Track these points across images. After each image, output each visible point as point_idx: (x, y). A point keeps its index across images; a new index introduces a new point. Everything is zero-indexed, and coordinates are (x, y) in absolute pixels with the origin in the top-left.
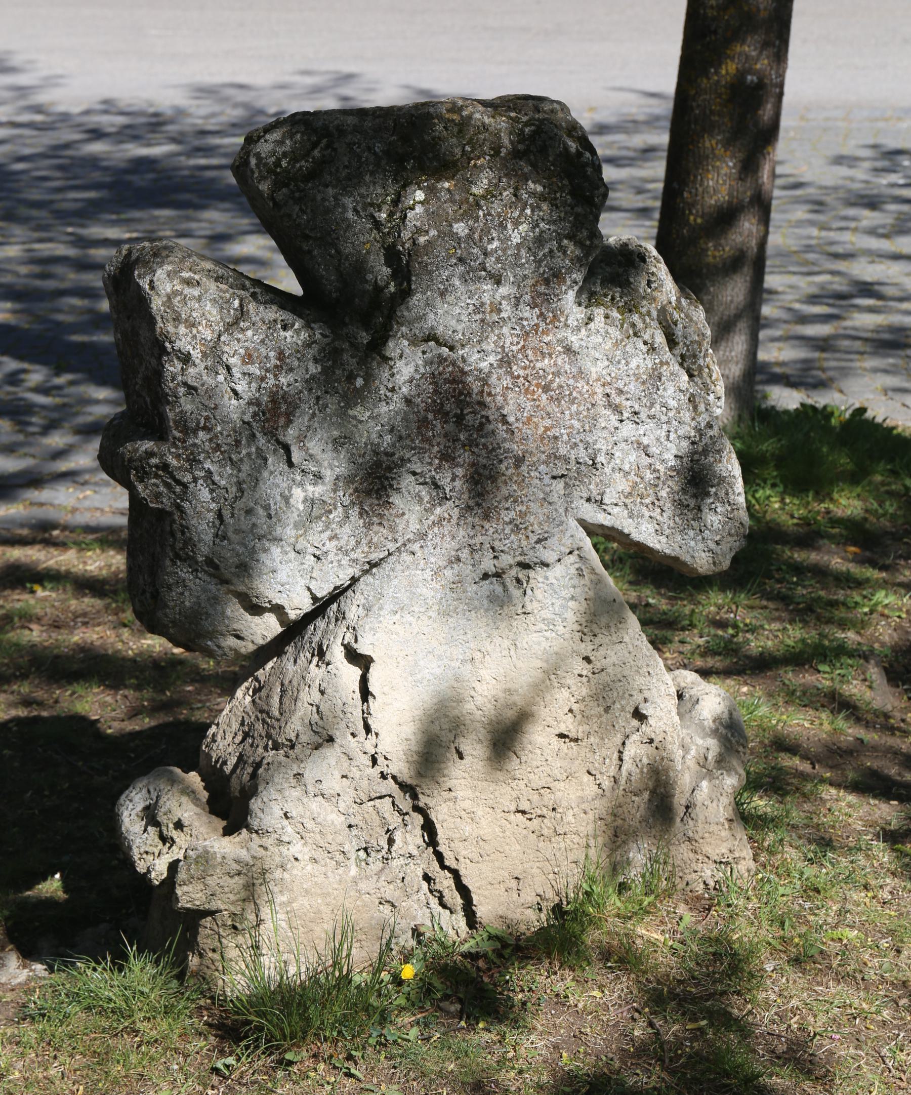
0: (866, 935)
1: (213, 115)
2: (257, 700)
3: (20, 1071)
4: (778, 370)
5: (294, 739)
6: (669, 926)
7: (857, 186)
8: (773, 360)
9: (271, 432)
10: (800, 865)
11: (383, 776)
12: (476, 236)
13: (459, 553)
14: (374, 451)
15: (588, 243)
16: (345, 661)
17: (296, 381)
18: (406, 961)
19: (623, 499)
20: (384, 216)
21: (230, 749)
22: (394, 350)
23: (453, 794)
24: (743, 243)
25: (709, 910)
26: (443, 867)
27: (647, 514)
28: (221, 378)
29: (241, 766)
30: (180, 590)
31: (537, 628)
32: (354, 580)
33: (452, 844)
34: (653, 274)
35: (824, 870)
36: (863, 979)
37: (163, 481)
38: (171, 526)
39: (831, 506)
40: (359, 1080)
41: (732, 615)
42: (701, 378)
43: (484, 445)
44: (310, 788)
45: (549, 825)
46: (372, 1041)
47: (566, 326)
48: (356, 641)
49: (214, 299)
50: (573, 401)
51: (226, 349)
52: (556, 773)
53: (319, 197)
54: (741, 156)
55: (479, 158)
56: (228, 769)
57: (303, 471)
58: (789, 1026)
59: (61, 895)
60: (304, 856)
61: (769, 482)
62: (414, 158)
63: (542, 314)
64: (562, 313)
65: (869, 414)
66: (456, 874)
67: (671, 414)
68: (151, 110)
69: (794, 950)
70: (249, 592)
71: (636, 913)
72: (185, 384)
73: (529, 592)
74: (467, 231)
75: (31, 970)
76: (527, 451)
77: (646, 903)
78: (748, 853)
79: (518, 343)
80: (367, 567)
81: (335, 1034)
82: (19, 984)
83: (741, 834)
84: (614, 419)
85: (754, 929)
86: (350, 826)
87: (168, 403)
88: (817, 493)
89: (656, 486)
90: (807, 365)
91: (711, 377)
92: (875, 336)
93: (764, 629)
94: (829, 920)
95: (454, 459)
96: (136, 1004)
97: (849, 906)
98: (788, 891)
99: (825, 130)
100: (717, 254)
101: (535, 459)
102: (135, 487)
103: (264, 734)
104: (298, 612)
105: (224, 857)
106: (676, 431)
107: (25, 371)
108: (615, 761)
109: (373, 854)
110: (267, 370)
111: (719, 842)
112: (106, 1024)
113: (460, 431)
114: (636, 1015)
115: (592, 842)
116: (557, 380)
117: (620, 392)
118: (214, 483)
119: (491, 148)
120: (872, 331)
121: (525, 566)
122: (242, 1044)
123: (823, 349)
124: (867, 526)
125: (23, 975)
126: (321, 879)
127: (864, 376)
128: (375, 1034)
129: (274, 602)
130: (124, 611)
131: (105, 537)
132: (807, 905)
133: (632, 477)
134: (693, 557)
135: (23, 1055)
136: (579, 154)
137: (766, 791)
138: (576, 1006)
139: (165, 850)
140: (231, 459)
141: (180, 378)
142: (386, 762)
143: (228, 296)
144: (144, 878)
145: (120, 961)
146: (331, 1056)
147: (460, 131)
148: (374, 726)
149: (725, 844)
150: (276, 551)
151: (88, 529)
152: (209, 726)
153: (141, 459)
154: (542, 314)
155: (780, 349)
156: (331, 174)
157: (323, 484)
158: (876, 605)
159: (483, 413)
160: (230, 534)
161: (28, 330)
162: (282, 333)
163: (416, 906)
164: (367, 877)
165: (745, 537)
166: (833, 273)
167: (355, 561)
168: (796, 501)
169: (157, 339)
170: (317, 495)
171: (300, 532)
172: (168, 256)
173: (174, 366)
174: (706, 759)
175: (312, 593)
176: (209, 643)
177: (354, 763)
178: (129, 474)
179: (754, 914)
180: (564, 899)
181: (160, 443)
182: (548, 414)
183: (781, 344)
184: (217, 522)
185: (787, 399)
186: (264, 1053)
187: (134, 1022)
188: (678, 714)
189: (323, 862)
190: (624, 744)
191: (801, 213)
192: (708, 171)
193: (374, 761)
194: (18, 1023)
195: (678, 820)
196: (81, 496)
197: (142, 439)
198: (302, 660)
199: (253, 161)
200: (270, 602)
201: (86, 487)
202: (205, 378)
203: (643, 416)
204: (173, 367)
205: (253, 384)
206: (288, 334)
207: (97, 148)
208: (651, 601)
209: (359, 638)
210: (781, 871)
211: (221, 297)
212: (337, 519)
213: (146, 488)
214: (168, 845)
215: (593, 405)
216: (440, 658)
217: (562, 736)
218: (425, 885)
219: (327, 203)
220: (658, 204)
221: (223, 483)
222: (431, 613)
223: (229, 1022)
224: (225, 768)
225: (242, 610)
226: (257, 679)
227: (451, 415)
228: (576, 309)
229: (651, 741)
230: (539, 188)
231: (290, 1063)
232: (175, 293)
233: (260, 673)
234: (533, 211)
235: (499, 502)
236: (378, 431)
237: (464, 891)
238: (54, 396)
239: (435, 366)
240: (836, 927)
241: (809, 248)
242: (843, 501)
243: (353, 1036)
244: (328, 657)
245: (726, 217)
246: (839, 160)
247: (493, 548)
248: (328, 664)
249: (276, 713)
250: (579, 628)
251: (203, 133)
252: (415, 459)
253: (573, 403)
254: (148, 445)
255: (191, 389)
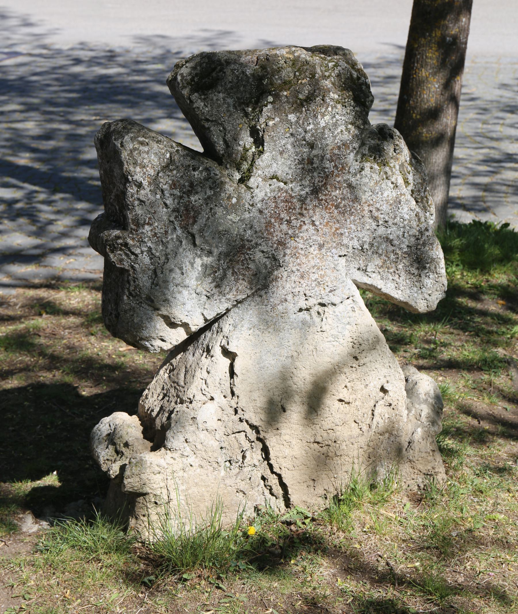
0: (509, 517)
1: (143, 53)
2: (172, 376)
3: (34, 581)
4: (459, 201)
5: (192, 398)
6: (399, 509)
7: (504, 100)
8: (456, 196)
9: (185, 227)
10: (472, 477)
11: (241, 420)
12: (301, 122)
13: (287, 297)
14: (241, 239)
15: (362, 127)
16: (222, 355)
17: (199, 199)
18: (251, 524)
19: (378, 269)
20: (250, 109)
21: (156, 403)
22: (254, 183)
23: (279, 431)
24: (443, 130)
25: (421, 501)
26: (273, 472)
27: (391, 278)
28: (158, 196)
29: (162, 412)
30: (132, 313)
31: (328, 340)
32: (228, 310)
33: (278, 460)
34: (397, 145)
35: (485, 481)
36: (507, 542)
37: (124, 252)
38: (128, 278)
39: (489, 278)
40: (224, 591)
41: (433, 337)
42: (422, 203)
43: (302, 237)
44: (200, 426)
45: (332, 450)
46: (232, 569)
47: (349, 172)
48: (228, 344)
49: (156, 153)
50: (351, 214)
51: (162, 180)
52: (337, 421)
53: (215, 98)
54: (442, 81)
55: (303, 79)
56: (154, 414)
57: (201, 249)
58: (465, 567)
59: (57, 484)
60: (196, 464)
61: (455, 263)
62: (268, 78)
63: (336, 166)
64: (347, 165)
65: (511, 227)
66: (279, 477)
67: (406, 223)
68: (108, 49)
69: (468, 525)
70: (170, 315)
71: (380, 502)
72: (139, 199)
73: (324, 319)
74: (296, 119)
75: (40, 525)
76: (325, 241)
77: (385, 496)
78: (442, 470)
79: (322, 181)
80: (235, 303)
81: (211, 564)
82: (33, 532)
83: (439, 458)
84: (374, 224)
85: (446, 512)
86: (221, 448)
87: (129, 209)
88: (482, 270)
89: (397, 262)
90: (476, 199)
91: (428, 203)
92: (513, 184)
93: (451, 345)
94: (488, 508)
95: (285, 244)
96: (99, 545)
97: (499, 501)
98: (465, 491)
99: (486, 68)
100: (428, 135)
101: (330, 246)
102: (109, 255)
103: (175, 395)
104: (197, 327)
105: (151, 463)
106: (408, 232)
107: (37, 192)
108: (371, 416)
109: (234, 464)
110: (184, 193)
111: (427, 463)
112: (82, 555)
113: (289, 229)
114: (380, 559)
115: (356, 461)
116: (343, 202)
117: (378, 210)
118: (152, 254)
119: (310, 74)
120: (512, 181)
121: (323, 305)
122: (159, 569)
123: (485, 190)
124: (510, 289)
125: (35, 528)
126: (204, 477)
127: (507, 206)
128: (233, 565)
129: (183, 321)
130: (92, 327)
131: (87, 283)
132: (476, 500)
133: (383, 257)
134: (416, 302)
135: (36, 572)
136: (358, 78)
137: (452, 435)
138: (346, 552)
139: (118, 458)
140: (162, 241)
141: (136, 196)
142: (243, 412)
143: (163, 151)
144: (106, 474)
145: (91, 521)
146: (208, 577)
147: (293, 64)
148: (236, 392)
149: (430, 464)
150: (185, 292)
151: (77, 280)
152: (144, 390)
153: (112, 240)
154: (336, 166)
155: (460, 190)
156: (222, 86)
157: (213, 256)
158: (514, 333)
159: (302, 219)
160: (160, 283)
161: (38, 169)
162: (192, 172)
163: (257, 494)
164: (230, 477)
165: (445, 292)
166: (490, 148)
167: (229, 299)
168: (470, 275)
169: (124, 174)
170: (209, 262)
171: (199, 283)
172: (131, 129)
173: (133, 189)
174: (420, 416)
175: (204, 317)
176: (147, 343)
177: (225, 412)
178: (105, 248)
179: (446, 504)
180: (339, 493)
181: (123, 231)
182: (338, 221)
183: (461, 187)
184: (153, 276)
185: (465, 218)
186: (171, 574)
187: (99, 555)
188: (406, 390)
189: (206, 468)
190: (375, 406)
191: (472, 115)
192: (424, 89)
193: (236, 412)
194: (33, 554)
195: (404, 450)
196: (68, 262)
197: (113, 228)
198: (197, 354)
199: (179, 78)
200: (181, 321)
201: (71, 257)
202: (149, 196)
203: (390, 223)
204: (132, 190)
205: (176, 200)
206: (196, 173)
207: (78, 69)
208: (388, 328)
209: (230, 343)
210: (461, 480)
211: (160, 152)
212: (220, 276)
213: (115, 256)
214: (120, 456)
215: (363, 217)
216: (274, 355)
217: (341, 400)
218: (262, 482)
219: (219, 102)
220: (395, 107)
221: (158, 254)
222: (270, 330)
223: (151, 556)
224: (153, 413)
225: (165, 325)
226: (172, 365)
227: (284, 220)
228: (355, 163)
229: (390, 405)
230: (336, 96)
231: (186, 580)
232: (135, 149)
233: (173, 361)
234: (332, 109)
235: (309, 269)
236: (244, 228)
237: (283, 486)
238: (53, 206)
239: (276, 193)
240: (492, 512)
241: (478, 135)
242: (496, 275)
243: (221, 566)
244: (212, 353)
245: (434, 114)
246: (504, 86)
247: (305, 294)
248: (212, 357)
249: (182, 383)
250: (352, 340)
251: (138, 62)
252: (263, 244)
253: (352, 215)
254: (116, 232)
255: (142, 202)
